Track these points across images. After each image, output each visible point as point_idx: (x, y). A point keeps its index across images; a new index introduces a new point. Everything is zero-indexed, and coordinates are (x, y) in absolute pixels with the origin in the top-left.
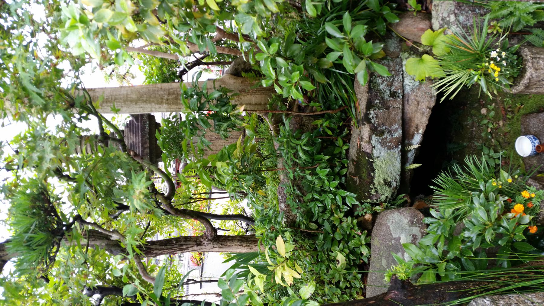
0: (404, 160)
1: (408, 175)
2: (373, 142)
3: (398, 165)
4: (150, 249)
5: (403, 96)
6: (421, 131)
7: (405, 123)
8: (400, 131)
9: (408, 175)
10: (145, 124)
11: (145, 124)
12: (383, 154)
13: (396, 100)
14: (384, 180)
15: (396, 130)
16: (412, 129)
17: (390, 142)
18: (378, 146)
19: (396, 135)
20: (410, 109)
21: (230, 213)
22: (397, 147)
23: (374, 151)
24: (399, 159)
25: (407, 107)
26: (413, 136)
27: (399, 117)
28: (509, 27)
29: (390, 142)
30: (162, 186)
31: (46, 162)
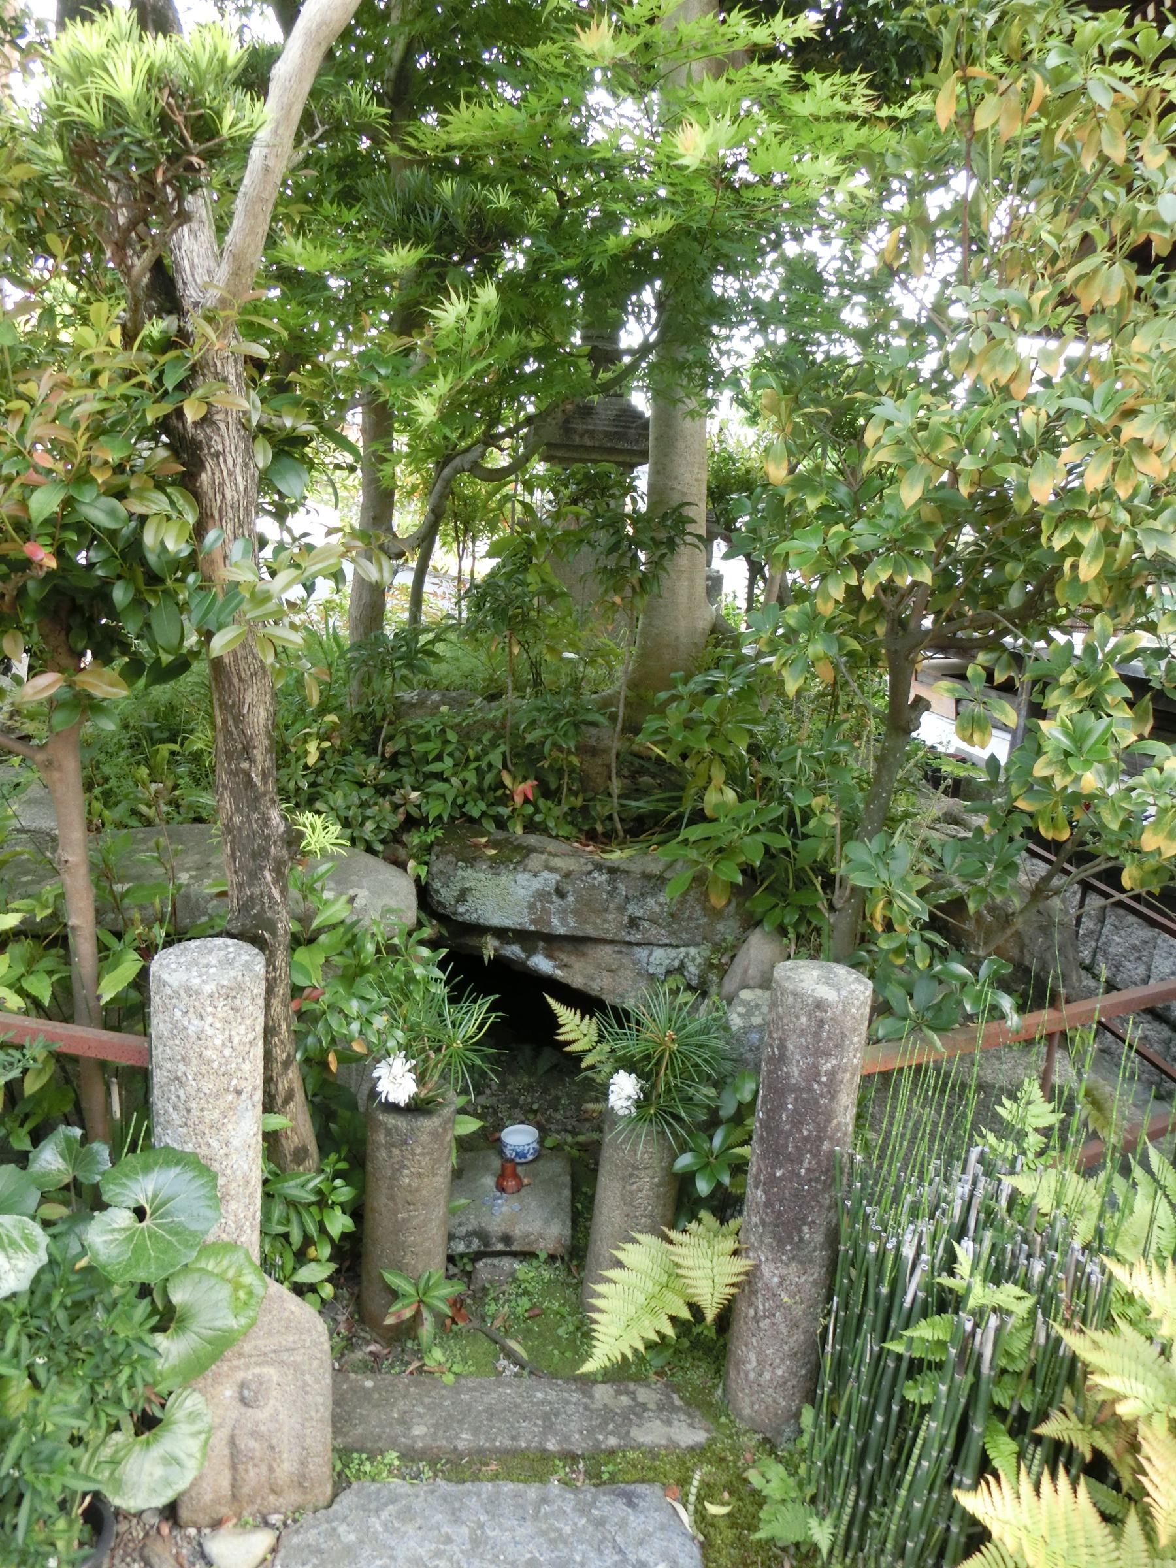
0: (501, 933)
1: (472, 941)
2: (546, 874)
3: (496, 921)
4: (381, 421)
5: (630, 944)
6: (558, 973)
7: (577, 942)
8: (562, 931)
9: (472, 941)
10: (628, 440)
11: (628, 440)
12: (522, 892)
13: (623, 927)
14: (470, 890)
15: (563, 921)
16: (564, 957)
17: (543, 909)
18: (537, 884)
19: (555, 922)
20: (605, 953)
21: (428, 579)
22: (533, 922)
23: (527, 876)
24: (508, 923)
25: (608, 949)
26: (550, 956)
27: (590, 931)
28: (133, 1149)
29: (543, 909)
30: (1022, 211)
31: (487, 313)
